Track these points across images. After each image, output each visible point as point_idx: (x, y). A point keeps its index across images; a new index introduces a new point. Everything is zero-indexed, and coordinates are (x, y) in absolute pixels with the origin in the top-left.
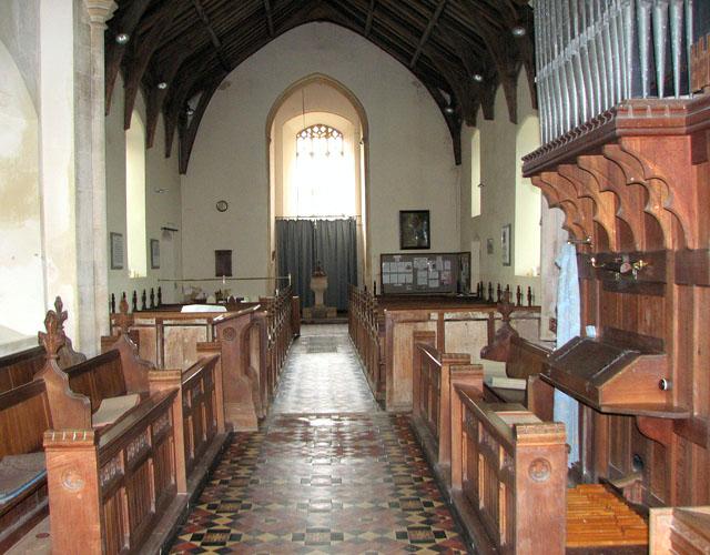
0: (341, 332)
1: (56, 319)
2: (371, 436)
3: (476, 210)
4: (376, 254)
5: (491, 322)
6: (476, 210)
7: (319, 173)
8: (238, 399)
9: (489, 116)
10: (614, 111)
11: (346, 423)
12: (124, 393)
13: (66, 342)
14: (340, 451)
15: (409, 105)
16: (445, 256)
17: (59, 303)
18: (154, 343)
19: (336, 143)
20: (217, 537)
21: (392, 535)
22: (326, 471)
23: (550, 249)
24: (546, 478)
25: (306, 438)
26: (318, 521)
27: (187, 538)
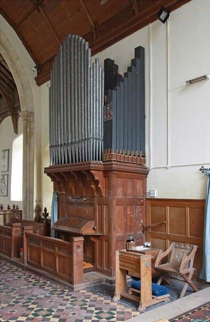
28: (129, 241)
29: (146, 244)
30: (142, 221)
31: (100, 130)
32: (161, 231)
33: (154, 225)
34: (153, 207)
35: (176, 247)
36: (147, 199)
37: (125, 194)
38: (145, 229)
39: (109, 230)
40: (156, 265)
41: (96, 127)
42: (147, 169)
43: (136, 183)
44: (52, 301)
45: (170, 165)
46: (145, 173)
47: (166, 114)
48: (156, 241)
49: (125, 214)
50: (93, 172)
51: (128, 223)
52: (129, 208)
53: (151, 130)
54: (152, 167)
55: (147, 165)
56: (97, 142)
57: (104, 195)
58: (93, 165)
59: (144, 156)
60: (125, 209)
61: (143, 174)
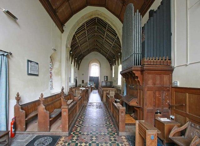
0: (97, 91)
1: (63, 89)
2: (101, 106)
3: (113, 76)
4: (101, 81)
5: (115, 91)
6: (113, 76)
7: (95, 71)
8: (85, 100)
9: (115, 64)
10: (132, 67)
11: (98, 104)
12: (71, 99)
13: (64, 92)
14: (97, 108)
15: (106, 63)
16: (109, 82)
17: (63, 87)
18: (75, 92)
19: (97, 66)
20: (82, 120)
21: (104, 120)
22: (95, 110)
23: (122, 82)
24: (123, 114)
25: (93, 106)
26: (95, 118)
27: (78, 120)
28: (157, 113)
29: (171, 117)
30: (168, 101)
31: (139, 49)
32: (182, 110)
33: (176, 105)
34: (176, 93)
35: (191, 126)
36: (172, 87)
37: (154, 84)
38: (170, 107)
39: (143, 106)
40: (171, 136)
41: (137, 47)
42: (172, 67)
43: (163, 77)
44: (104, 138)
45: (189, 63)
46: (171, 70)
47: (186, 30)
48: (178, 116)
49: (155, 97)
50: (134, 72)
51: (157, 102)
52: (157, 93)
53: (176, 41)
54: (176, 65)
55: (172, 65)
56: (136, 55)
57: (141, 84)
58: (134, 68)
59: (170, 60)
60: (155, 93)
61: (168, 71)
